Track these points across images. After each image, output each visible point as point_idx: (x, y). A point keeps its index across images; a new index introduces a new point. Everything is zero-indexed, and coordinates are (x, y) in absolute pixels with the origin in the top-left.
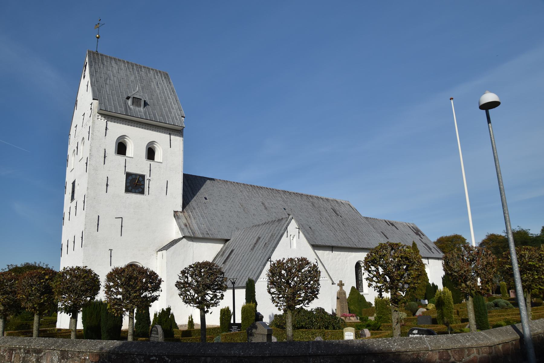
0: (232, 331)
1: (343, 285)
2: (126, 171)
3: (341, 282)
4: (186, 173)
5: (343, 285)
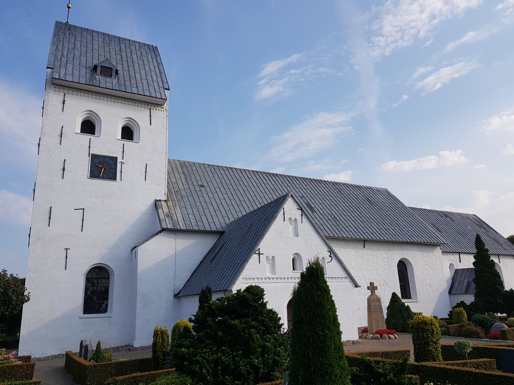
0: (166, 365)
1: (376, 288)
2: (91, 152)
3: (372, 284)
4: (172, 158)
5: (376, 288)
